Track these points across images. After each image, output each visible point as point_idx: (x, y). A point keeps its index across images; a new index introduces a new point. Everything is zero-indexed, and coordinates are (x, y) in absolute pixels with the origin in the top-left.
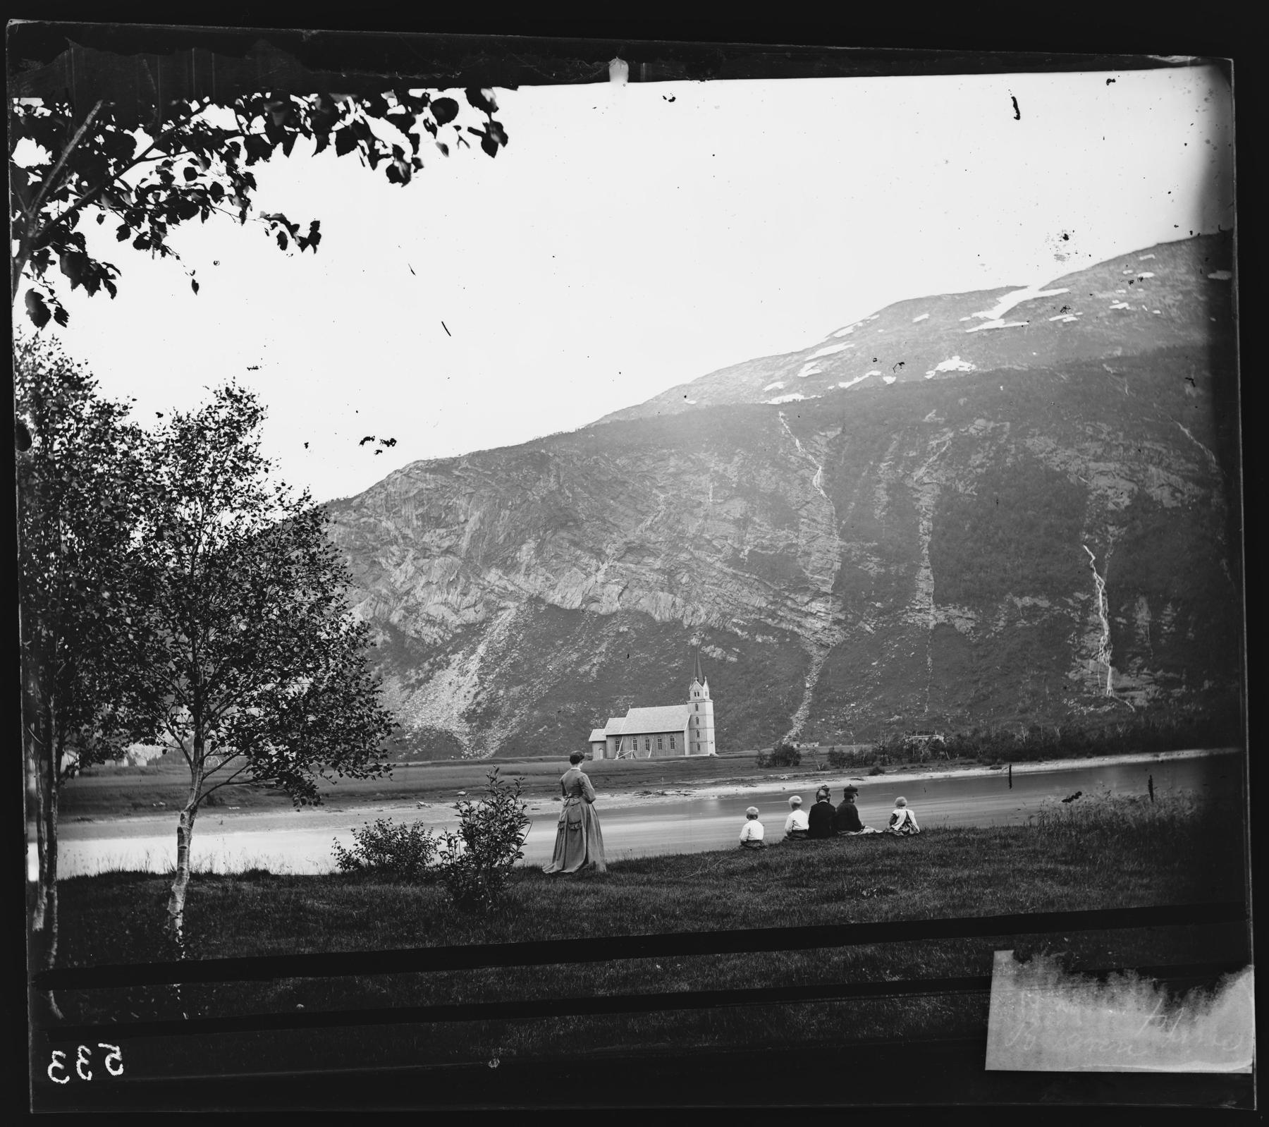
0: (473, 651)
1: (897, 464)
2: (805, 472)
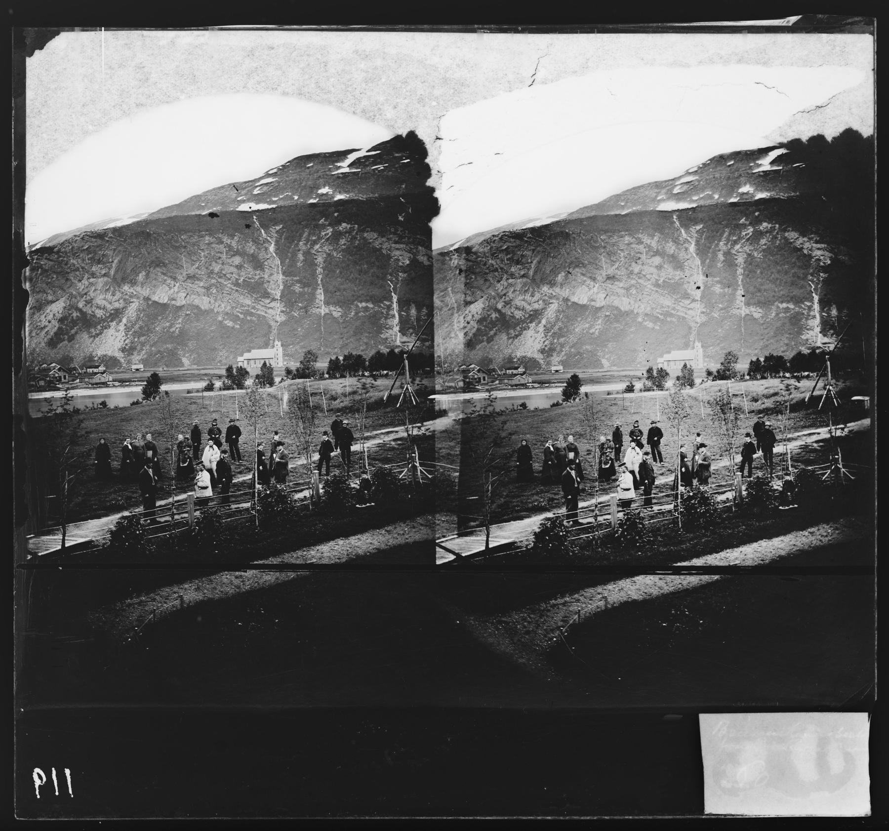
0: (121, 321)
1: (307, 243)
2: (266, 245)
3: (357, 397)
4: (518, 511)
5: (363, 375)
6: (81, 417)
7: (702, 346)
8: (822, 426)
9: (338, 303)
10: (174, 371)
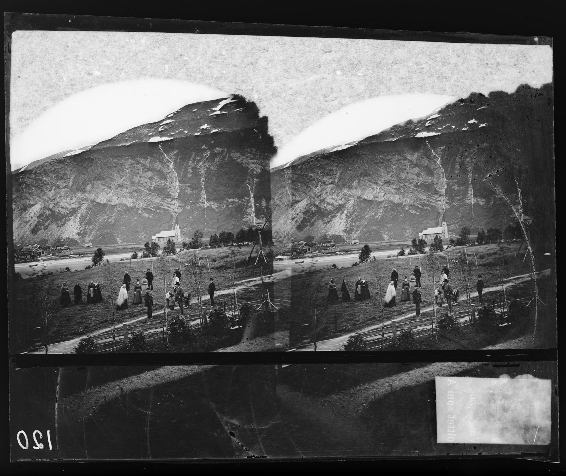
2: (435, 160)
3: (229, 260)
4: (65, 336)
5: (232, 245)
6: (322, 274)
7: (180, 228)
8: (257, 276)
9: (215, 200)
10: (113, 247)
